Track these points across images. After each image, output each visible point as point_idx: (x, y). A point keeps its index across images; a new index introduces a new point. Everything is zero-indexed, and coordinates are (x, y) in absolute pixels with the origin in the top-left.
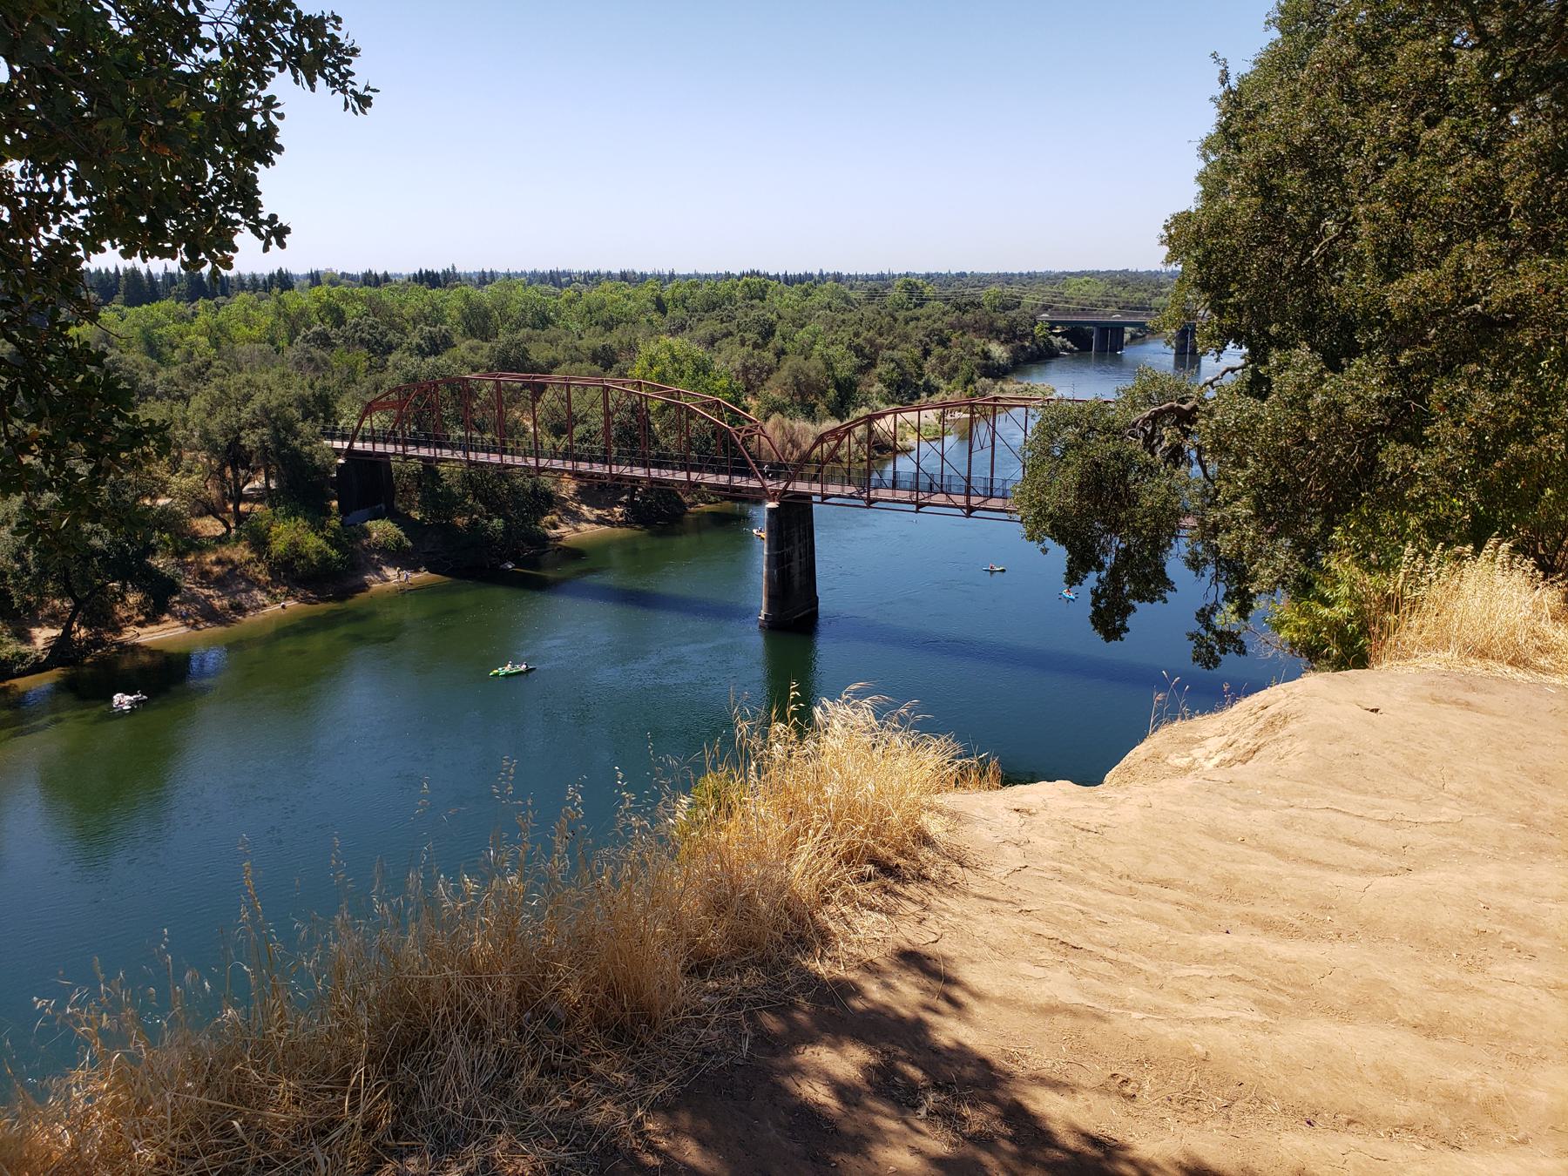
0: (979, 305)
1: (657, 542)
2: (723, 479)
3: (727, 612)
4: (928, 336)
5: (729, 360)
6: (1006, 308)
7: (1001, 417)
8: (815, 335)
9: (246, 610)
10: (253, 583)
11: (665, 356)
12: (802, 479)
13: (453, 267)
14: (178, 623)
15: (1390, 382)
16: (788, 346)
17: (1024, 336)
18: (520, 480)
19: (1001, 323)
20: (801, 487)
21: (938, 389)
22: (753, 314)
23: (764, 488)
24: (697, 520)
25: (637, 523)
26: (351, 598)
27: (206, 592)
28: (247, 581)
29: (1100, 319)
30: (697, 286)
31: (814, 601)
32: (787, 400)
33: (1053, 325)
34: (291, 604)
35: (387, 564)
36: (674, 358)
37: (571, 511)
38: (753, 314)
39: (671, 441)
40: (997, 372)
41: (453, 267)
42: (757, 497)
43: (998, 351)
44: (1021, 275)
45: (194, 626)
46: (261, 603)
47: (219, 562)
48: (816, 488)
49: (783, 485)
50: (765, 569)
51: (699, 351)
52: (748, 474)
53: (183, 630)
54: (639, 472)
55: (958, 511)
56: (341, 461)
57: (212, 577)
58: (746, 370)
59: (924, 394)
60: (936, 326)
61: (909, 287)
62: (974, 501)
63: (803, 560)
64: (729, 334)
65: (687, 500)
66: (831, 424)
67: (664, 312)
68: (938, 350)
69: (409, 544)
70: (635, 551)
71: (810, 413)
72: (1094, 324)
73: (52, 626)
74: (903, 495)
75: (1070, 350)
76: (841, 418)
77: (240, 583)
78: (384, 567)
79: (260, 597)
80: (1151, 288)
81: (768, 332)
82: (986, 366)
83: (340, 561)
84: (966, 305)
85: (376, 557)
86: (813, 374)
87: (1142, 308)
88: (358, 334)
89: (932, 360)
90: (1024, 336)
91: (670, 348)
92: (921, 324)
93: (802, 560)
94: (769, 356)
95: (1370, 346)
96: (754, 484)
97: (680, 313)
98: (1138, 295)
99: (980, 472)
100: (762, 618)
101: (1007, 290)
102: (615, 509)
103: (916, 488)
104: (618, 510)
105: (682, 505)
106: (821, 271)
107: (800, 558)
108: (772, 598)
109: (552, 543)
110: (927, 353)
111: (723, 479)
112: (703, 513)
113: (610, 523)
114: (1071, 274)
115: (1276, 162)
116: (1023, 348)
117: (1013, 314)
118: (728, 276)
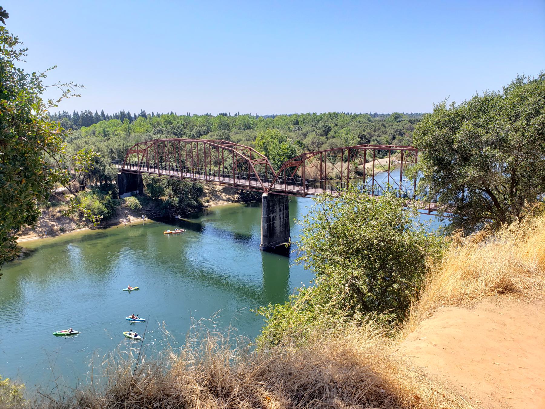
4: (395, 132)
9: (66, 231)
10: (72, 220)
13: (238, 113)
14: (35, 235)
18: (188, 183)
25: (242, 201)
26: (110, 227)
27: (52, 223)
28: (70, 219)
34: (86, 229)
35: (130, 214)
37: (218, 196)
41: (238, 113)
45: (41, 237)
46: (73, 228)
47: (59, 212)
53: (37, 238)
56: (120, 173)
57: (55, 217)
60: (398, 128)
61: (397, 116)
63: (282, 220)
68: (398, 137)
69: (141, 207)
73: (524, 202)
77: (67, 220)
78: (129, 216)
79: (73, 226)
83: (108, 213)
84: (415, 121)
85: (126, 211)
88: (173, 130)
89: (395, 141)
92: (393, 127)
93: (281, 220)
102: (235, 195)
104: (236, 196)
106: (371, 113)
107: (280, 219)
109: (205, 208)
110: (394, 138)
113: (232, 201)
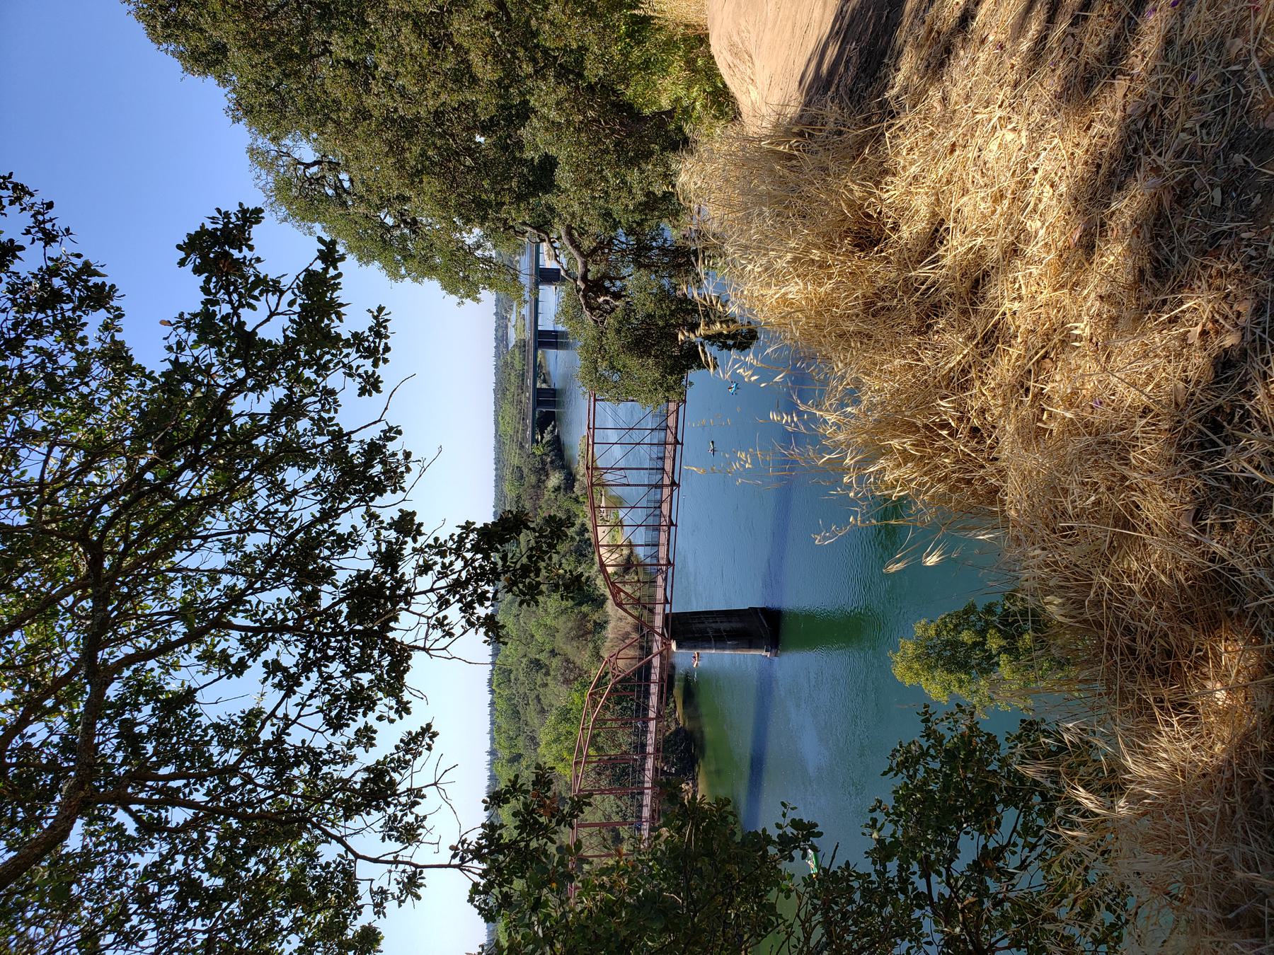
0: (519, 497)
1: (709, 752)
2: (654, 689)
3: (765, 688)
5: (559, 695)
6: (522, 477)
7: (599, 464)
8: (539, 625)
11: (555, 747)
12: (653, 622)
15: (544, 78)
16: (548, 647)
17: (543, 462)
19: (533, 479)
20: (658, 621)
21: (583, 525)
22: (522, 678)
23: (661, 653)
24: (690, 718)
29: (531, 406)
30: (499, 727)
31: (753, 611)
32: (591, 645)
33: (535, 441)
36: (557, 740)
38: (522, 678)
39: (625, 739)
40: (570, 479)
42: (665, 655)
43: (555, 479)
44: (496, 469)
48: (659, 609)
49: (657, 637)
50: (727, 652)
51: (552, 718)
52: (649, 666)
54: (650, 763)
55: (675, 493)
58: (567, 682)
59: (587, 535)
62: (667, 481)
64: (538, 698)
65: (673, 727)
66: (610, 606)
67: (520, 756)
70: (718, 772)
71: (601, 626)
72: (534, 410)
74: (663, 538)
75: (554, 427)
76: (605, 600)
80: (508, 370)
81: (537, 664)
82: (565, 489)
86: (570, 625)
87: (522, 377)
90: (543, 462)
91: (548, 744)
94: (555, 663)
95: (522, 94)
96: (656, 662)
97: (521, 742)
98: (513, 379)
99: (644, 477)
100: (768, 654)
101: (508, 477)
103: (657, 528)
105: (677, 732)
108: (751, 645)
111: (654, 689)
112: (684, 713)
114: (497, 431)
115: (400, 165)
116: (552, 462)
117: (526, 471)
118: (492, 704)
